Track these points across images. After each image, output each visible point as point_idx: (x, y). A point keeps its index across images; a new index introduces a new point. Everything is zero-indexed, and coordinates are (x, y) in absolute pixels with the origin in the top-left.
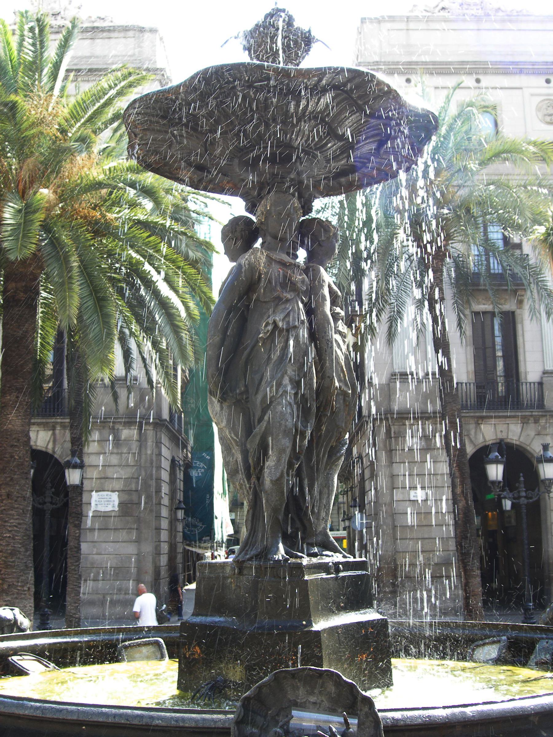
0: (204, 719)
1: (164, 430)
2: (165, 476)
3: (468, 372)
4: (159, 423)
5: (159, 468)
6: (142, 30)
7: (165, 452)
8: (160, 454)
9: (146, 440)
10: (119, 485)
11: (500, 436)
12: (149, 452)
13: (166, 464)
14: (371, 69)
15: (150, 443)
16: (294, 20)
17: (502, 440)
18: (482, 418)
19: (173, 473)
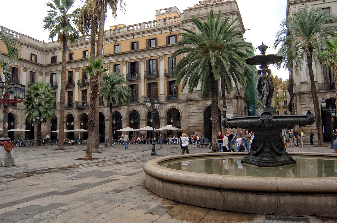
0: (278, 121)
1: (243, 99)
2: (243, 110)
3: (322, 81)
4: (242, 98)
5: (242, 108)
6: (231, 2)
7: (243, 104)
8: (242, 105)
9: (238, 102)
10: (232, 112)
11: (331, 97)
12: (239, 105)
13: (244, 107)
14: (216, 30)
15: (240, 102)
16: (175, 7)
17: (332, 98)
18: (326, 92)
19: (245, 109)
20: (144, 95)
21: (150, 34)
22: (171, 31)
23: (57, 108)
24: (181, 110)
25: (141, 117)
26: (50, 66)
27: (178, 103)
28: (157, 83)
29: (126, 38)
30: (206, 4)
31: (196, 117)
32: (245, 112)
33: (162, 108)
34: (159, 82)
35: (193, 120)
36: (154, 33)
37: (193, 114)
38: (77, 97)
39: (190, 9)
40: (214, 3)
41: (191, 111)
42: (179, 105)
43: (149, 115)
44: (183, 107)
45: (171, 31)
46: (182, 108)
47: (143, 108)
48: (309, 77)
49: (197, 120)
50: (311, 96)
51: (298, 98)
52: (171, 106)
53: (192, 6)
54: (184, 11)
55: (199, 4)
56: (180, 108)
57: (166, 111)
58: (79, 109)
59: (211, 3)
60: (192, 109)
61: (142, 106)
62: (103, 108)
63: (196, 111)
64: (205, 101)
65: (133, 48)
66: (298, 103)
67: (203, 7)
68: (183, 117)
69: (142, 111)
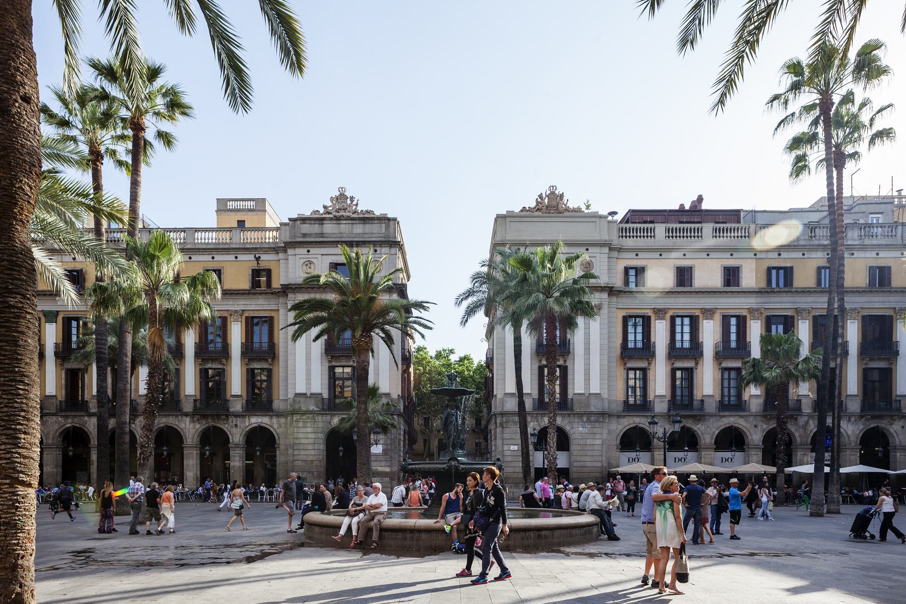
2: (402, 438)
13: (402, 433)
20: (193, 393)
21: (209, 258)
22: (258, 259)
23: (185, 410)
24: (278, 431)
25: (703, 442)
26: (249, 294)
27: (271, 416)
28: (224, 370)
29: (855, 253)
30: (337, 214)
31: (310, 447)
32: (404, 441)
33: (236, 426)
34: (182, 368)
35: (303, 452)
36: (882, 254)
37: (303, 441)
38: (708, 382)
39: (304, 220)
40: (355, 216)
41: (301, 436)
42: (274, 420)
43: (770, 438)
44: (283, 426)
45: (258, 259)
46: (281, 427)
47: (190, 422)
48: (536, 387)
49: (313, 452)
50: (517, 419)
51: (499, 421)
52: (255, 421)
53: (307, 213)
54: (290, 219)
55: (322, 211)
56: (276, 426)
57: (244, 433)
58: (198, 413)
59: (348, 214)
60: (302, 430)
61: (188, 419)
62: (86, 418)
63: (310, 436)
64: (329, 417)
65: (255, 284)
66: (499, 430)
67: (331, 219)
68: (282, 447)
69: (851, 430)
